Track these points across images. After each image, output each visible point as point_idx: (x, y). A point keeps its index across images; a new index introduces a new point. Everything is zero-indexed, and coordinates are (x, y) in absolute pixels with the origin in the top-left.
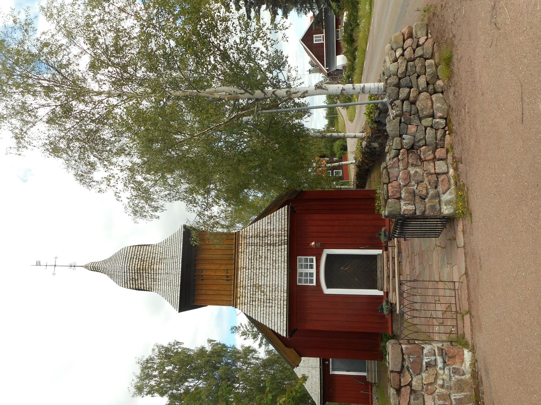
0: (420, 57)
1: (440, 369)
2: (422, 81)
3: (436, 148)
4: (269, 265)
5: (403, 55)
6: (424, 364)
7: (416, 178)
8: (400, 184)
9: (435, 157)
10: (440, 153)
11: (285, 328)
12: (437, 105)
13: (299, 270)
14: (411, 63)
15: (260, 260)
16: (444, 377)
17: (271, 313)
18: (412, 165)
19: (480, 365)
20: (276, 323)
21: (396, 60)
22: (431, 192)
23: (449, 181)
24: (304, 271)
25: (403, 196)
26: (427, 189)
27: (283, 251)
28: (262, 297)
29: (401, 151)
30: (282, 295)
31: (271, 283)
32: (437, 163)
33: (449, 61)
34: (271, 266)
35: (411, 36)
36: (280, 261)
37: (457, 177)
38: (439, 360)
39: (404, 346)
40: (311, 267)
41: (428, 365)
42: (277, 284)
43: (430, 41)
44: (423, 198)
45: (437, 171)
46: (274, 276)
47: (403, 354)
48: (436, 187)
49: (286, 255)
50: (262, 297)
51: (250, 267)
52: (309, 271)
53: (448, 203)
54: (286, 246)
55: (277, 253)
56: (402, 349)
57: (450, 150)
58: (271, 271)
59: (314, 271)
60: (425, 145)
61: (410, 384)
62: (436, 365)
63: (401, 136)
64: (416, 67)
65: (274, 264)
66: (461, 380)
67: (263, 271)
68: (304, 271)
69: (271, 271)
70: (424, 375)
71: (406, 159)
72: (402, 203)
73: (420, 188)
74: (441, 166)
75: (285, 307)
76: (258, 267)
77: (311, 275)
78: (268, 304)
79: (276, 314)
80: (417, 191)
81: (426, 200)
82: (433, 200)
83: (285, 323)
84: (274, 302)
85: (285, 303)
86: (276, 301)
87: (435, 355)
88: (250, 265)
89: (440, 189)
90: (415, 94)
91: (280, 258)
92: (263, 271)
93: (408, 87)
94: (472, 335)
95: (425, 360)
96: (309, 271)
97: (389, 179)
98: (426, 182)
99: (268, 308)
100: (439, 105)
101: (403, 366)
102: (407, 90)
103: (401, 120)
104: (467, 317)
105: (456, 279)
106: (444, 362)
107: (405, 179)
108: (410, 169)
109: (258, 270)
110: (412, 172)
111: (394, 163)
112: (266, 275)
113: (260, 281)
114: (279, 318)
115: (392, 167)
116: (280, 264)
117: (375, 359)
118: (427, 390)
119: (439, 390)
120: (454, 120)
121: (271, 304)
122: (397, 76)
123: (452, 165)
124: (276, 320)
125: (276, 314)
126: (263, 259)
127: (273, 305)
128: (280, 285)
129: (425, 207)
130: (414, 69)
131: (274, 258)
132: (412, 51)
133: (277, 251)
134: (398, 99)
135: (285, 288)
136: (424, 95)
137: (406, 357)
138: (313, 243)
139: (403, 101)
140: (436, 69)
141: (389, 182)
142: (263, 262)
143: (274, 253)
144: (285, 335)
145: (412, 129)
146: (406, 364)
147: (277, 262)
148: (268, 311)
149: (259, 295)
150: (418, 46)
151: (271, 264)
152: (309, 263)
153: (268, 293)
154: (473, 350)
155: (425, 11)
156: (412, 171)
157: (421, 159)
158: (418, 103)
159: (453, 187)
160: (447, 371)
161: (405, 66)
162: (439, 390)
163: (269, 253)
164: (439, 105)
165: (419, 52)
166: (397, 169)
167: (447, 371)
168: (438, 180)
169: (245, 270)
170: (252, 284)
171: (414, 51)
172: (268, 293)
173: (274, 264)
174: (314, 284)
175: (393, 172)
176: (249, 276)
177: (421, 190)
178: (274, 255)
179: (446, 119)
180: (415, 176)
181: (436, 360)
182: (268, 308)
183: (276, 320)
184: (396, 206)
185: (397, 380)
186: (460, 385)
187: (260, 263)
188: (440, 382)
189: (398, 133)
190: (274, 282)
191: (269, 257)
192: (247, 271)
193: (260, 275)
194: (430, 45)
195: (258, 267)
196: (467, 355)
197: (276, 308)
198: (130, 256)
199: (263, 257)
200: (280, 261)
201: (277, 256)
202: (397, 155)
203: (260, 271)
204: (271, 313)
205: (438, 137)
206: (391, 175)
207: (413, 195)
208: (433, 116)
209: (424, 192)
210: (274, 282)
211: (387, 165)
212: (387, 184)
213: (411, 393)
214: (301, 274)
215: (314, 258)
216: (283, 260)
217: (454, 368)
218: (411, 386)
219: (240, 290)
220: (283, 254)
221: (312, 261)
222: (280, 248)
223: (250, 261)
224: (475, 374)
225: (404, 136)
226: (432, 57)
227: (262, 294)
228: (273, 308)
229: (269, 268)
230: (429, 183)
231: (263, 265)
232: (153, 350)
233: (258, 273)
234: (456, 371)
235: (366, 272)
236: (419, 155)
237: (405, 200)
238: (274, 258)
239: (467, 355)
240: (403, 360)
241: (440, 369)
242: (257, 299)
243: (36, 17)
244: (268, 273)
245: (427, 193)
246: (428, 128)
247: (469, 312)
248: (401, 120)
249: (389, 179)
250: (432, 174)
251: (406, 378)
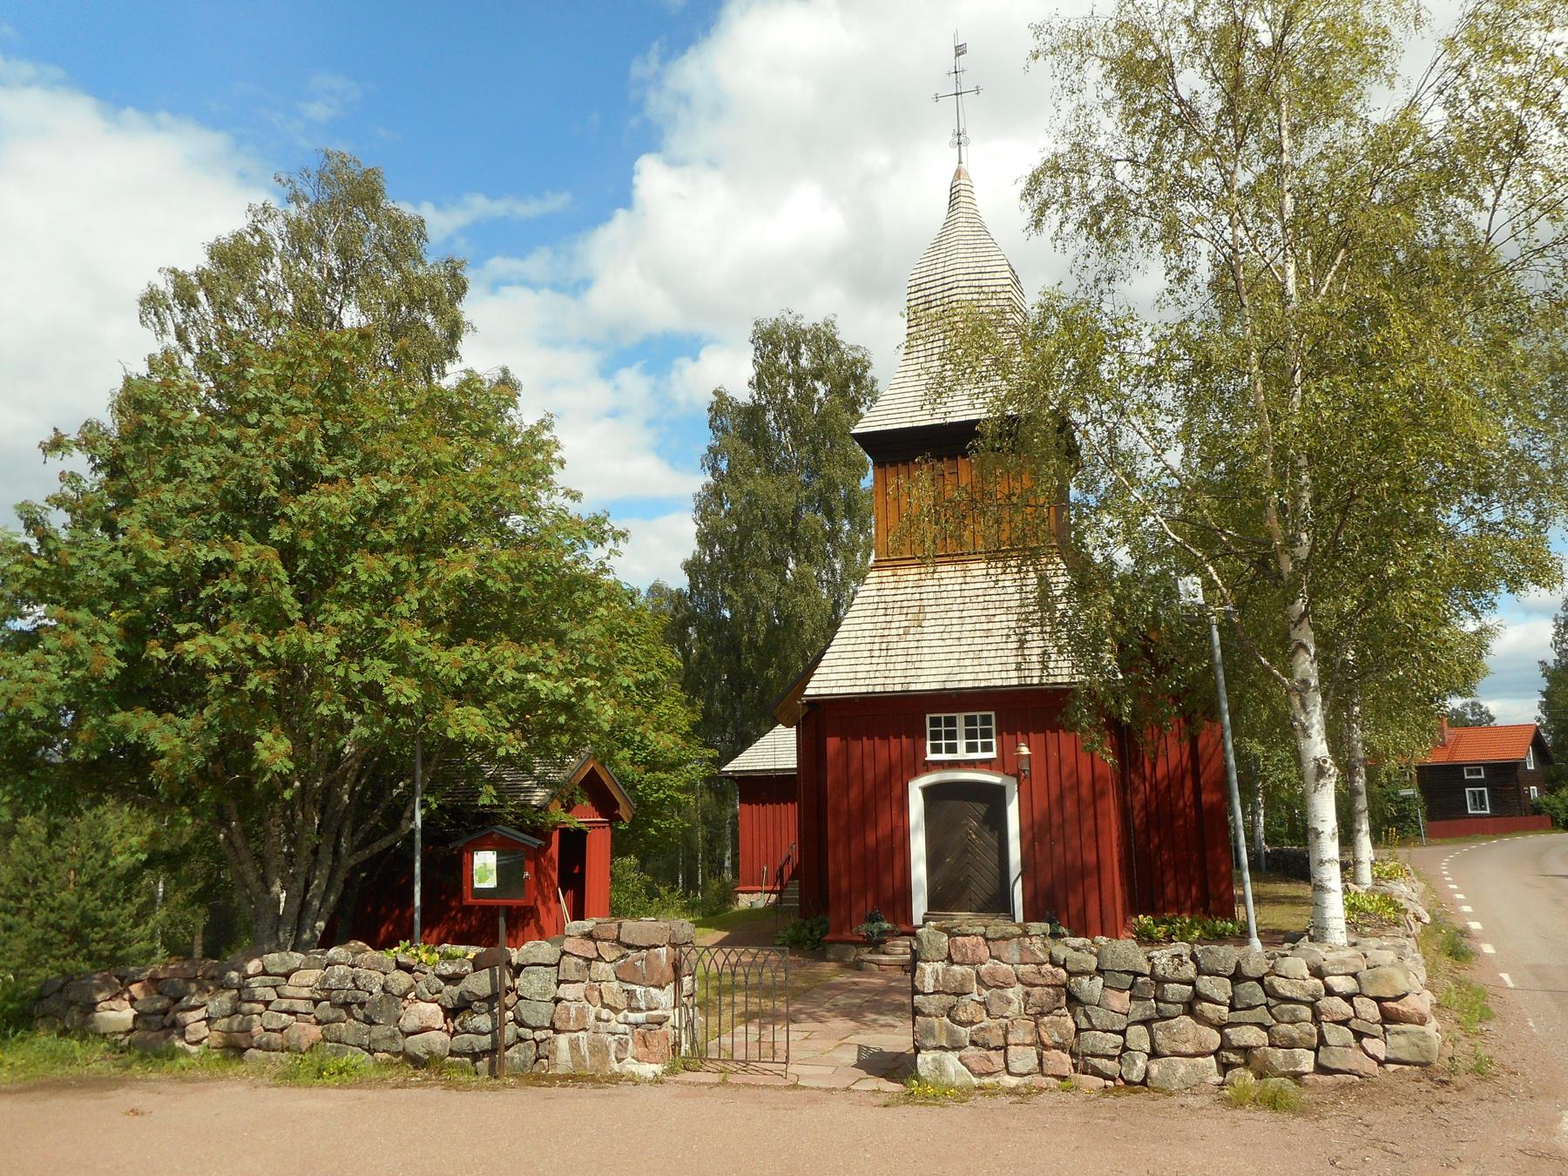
0: (1321, 1036)
1: (626, 1017)
2: (1250, 1036)
3: (1073, 1054)
4: (969, 641)
5: (1330, 992)
6: (633, 987)
7: (995, 1001)
8: (982, 963)
9: (1045, 1047)
10: (1061, 1061)
11: (823, 691)
12: (1182, 1066)
13: (960, 718)
14: (1306, 1012)
15: (983, 619)
16: (613, 1023)
17: (858, 654)
18: (1028, 994)
19: (627, 1088)
20: (835, 670)
21: (1317, 972)
22: (965, 1033)
23: (989, 1074)
24: (961, 728)
25: (955, 967)
26: (972, 1023)
27: (1004, 675)
28: (894, 632)
29: (1061, 971)
30: (896, 680)
31: (926, 650)
32: (1033, 1052)
33: (1273, 1103)
34: (966, 648)
35: (1388, 1018)
36: (977, 669)
37: (992, 1092)
38: (639, 1017)
39: (663, 951)
40: (971, 748)
41: (631, 995)
42: (924, 665)
43: (1370, 1067)
44: (950, 1012)
45: (1011, 1049)
46: (942, 656)
47: (647, 948)
48: (973, 1043)
49: (992, 683)
50: (894, 632)
51: (965, 593)
52: (961, 744)
53: (939, 1066)
54: (1015, 682)
55: (998, 660)
56: (656, 947)
57: (1065, 1084)
58: (953, 649)
59: (962, 754)
60: (1078, 1030)
61: (600, 958)
62: (632, 1010)
63: (1100, 971)
64: (1293, 1023)
65: (971, 655)
66: (608, 1054)
67: (955, 628)
68: (961, 728)
69: (953, 649)
70: (616, 984)
71: (1041, 981)
72: (940, 966)
73: (972, 1008)
74: (1023, 1058)
75: (870, 689)
76: (965, 614)
77: (952, 749)
78: (877, 646)
79: (854, 668)
80: (966, 999)
81: (946, 1020)
82: (945, 1034)
83: (835, 691)
84: (882, 660)
85: (878, 689)
86: (883, 667)
87: (649, 1009)
88: (971, 593)
89: (971, 1051)
90: (1211, 1015)
91: (985, 668)
92: (955, 628)
93: (1232, 999)
94: (684, 1083)
95: (639, 990)
96: (961, 744)
97: (993, 940)
98: (987, 1022)
99: (869, 647)
100: (1182, 1070)
101: (629, 947)
102: (1224, 998)
103: (1143, 975)
104: (716, 1078)
105: (793, 1069)
106: (637, 1025)
107: (992, 976)
108: (1019, 987)
109: (958, 614)
110: (1010, 993)
111: (1033, 953)
112: (945, 636)
113: (933, 622)
114: (844, 676)
115: (1022, 948)
116: (969, 669)
117: (800, 901)
118: (591, 988)
119: (592, 1011)
120: (1135, 1100)
121: (876, 653)
122: (1267, 974)
123: (1025, 1085)
124: (841, 669)
125: (854, 668)
126: (985, 626)
127: (874, 660)
128: (919, 672)
129: (930, 1015)
130: (1286, 1018)
131: (985, 654)
132: (1340, 1017)
133: (1004, 660)
134: (1200, 972)
135: (913, 687)
136: (1214, 1039)
137: (644, 953)
138: (1025, 751)
139: (1192, 983)
140: (1284, 1075)
141: (987, 940)
142: (978, 626)
143: (1000, 653)
144: (807, 692)
145: (1120, 1001)
146: (633, 954)
147: (976, 662)
148: (862, 647)
149: (899, 621)
150: (1359, 1035)
151: (973, 648)
152: (979, 741)
153: (902, 645)
154: (657, 1081)
155: (1451, 1059)
156: (1015, 993)
157: (1042, 1014)
158: (1188, 1019)
159: (976, 1081)
160: (622, 1028)
161: (1294, 995)
162: (592, 1011)
163: (998, 639)
164: (1182, 1070)
165: (1336, 1035)
166: (1017, 958)
167: (622, 1028)
168: (990, 1049)
169: (960, 580)
170: (925, 602)
171: (1345, 1023)
172: (902, 645)
173: (971, 655)
174: (931, 757)
175: (1011, 950)
176: (944, 595)
177: (968, 1008)
178: (993, 653)
179: (1144, 1083)
180: (1000, 997)
181: (639, 1010)
182: (869, 647)
183: (841, 669)
184: (934, 953)
185: (606, 935)
186: (600, 1051)
187: (974, 620)
188: (605, 1013)
189: (1108, 966)
190: (928, 657)
191: (990, 640)
192: (957, 587)
193: (947, 622)
194: (1354, 1066)
195: (965, 614)
196: (648, 1070)
197: (868, 668)
198: (983, 283)
199: (990, 626)
200: (977, 669)
201: (990, 661)
202: (1054, 963)
203: (955, 621)
204: (858, 654)
205: (1096, 1061)
206: (1003, 944)
207: (959, 990)
208: (1154, 1054)
209: (963, 1017)
210: (928, 657)
211: (1030, 937)
212: (983, 936)
213: (586, 959)
214: (951, 722)
215: (993, 755)
216: (981, 676)
217: (627, 1042)
218: (596, 960)
219: (911, 574)
220: (996, 675)
221: (987, 747)
222: (1009, 667)
223: (980, 592)
224: (616, 1078)
225: (1099, 981)
226: (1321, 1069)
227: (901, 631)
228: (868, 661)
229: (963, 641)
230: (983, 1029)
231: (970, 627)
232: (857, 348)
233: (950, 614)
234: (622, 1045)
235: (966, 886)
236: (1050, 1012)
237: (946, 971)
238: (985, 654)
239: (648, 1070)
240: (639, 948)
241: (626, 1017)
242: (889, 618)
243: (617, 388)
244: (949, 642)
245: (961, 1024)
246: (1120, 1039)
247: (724, 1082)
248: (1143, 975)
249: (993, 940)
250: (1006, 1038)
251: (610, 952)
